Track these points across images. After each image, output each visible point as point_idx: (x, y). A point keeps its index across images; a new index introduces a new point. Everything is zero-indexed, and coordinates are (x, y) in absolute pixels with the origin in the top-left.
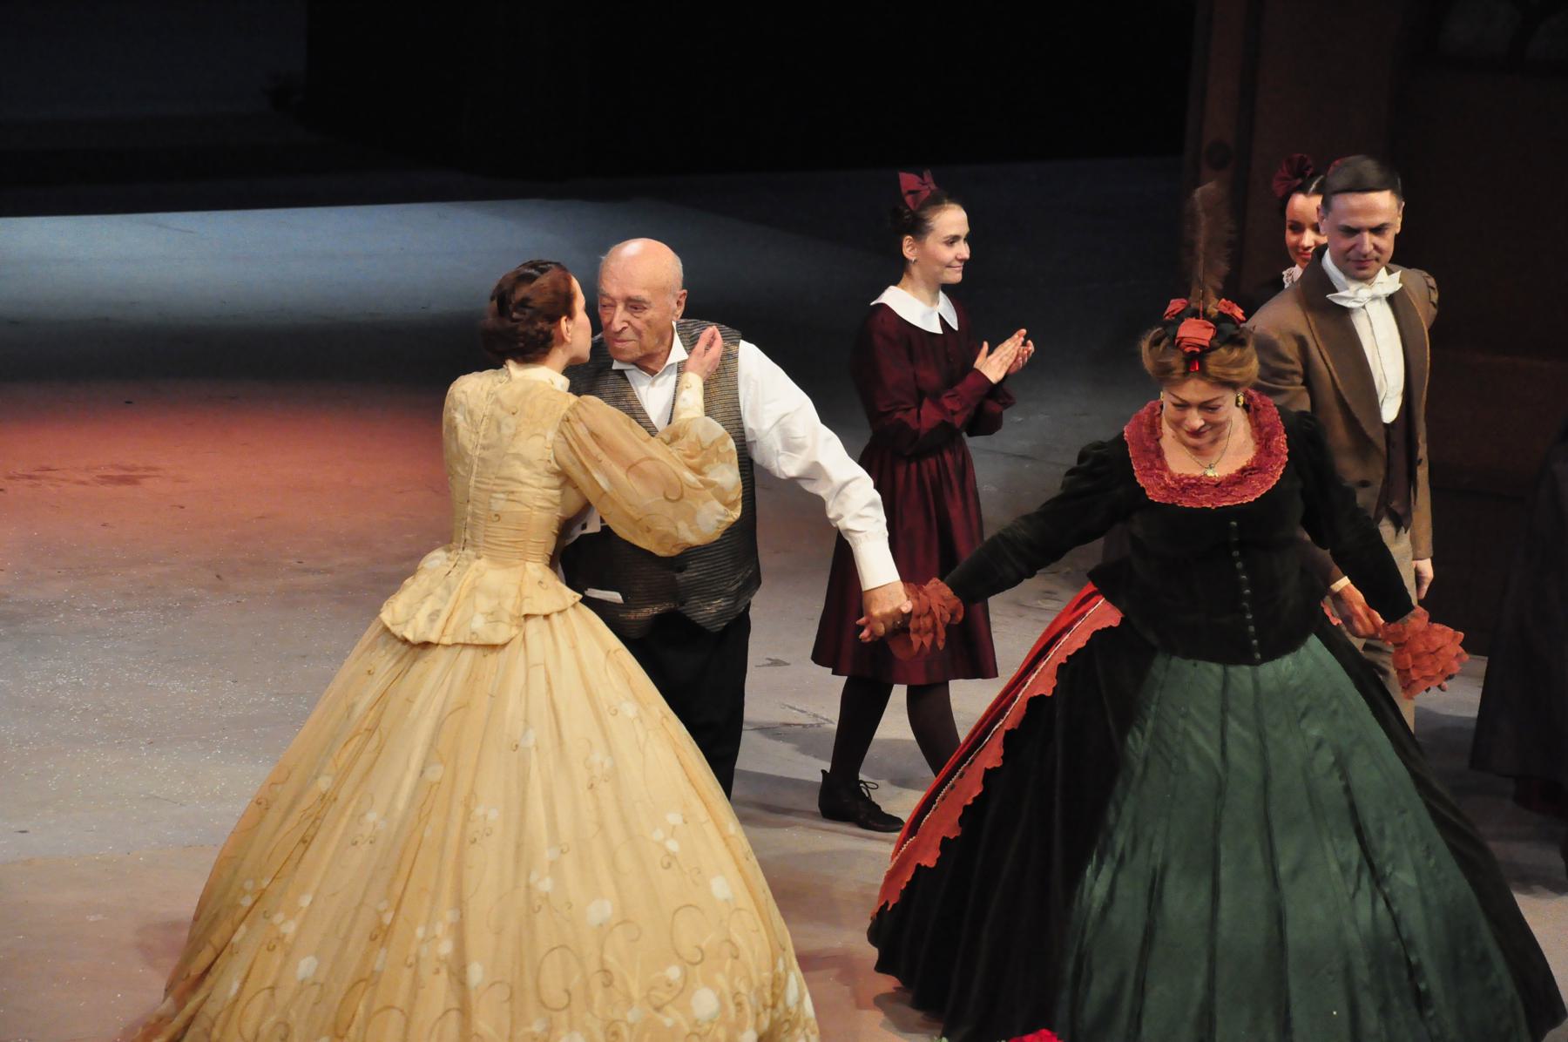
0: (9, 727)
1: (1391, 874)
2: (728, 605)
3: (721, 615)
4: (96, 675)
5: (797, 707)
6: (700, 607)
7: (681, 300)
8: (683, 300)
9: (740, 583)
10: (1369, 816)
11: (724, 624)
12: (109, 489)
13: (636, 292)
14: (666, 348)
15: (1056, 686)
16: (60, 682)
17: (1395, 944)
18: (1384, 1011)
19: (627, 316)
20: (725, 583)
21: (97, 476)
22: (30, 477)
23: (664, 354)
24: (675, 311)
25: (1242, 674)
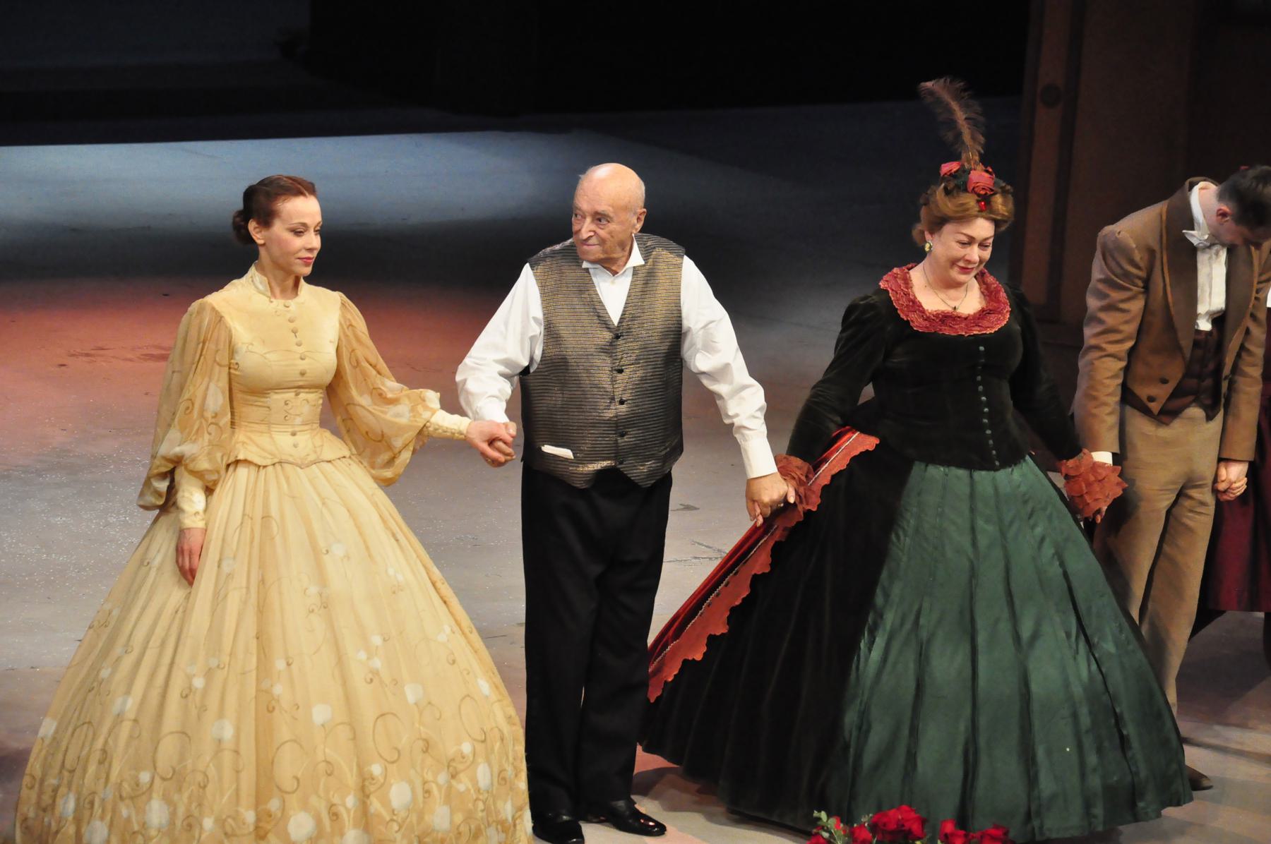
0: (70, 556)
1: (1098, 643)
2: (657, 466)
3: (651, 474)
4: (139, 515)
5: (704, 543)
6: (635, 466)
7: (641, 217)
8: (643, 218)
9: (668, 449)
10: (1080, 595)
11: (653, 482)
12: (152, 365)
13: (602, 208)
14: (627, 253)
15: (844, 470)
16: (112, 520)
17: (1105, 698)
18: (1100, 750)
19: (593, 227)
20: (657, 448)
21: (142, 355)
22: (87, 355)
23: (624, 259)
24: (634, 225)
25: (983, 477)
